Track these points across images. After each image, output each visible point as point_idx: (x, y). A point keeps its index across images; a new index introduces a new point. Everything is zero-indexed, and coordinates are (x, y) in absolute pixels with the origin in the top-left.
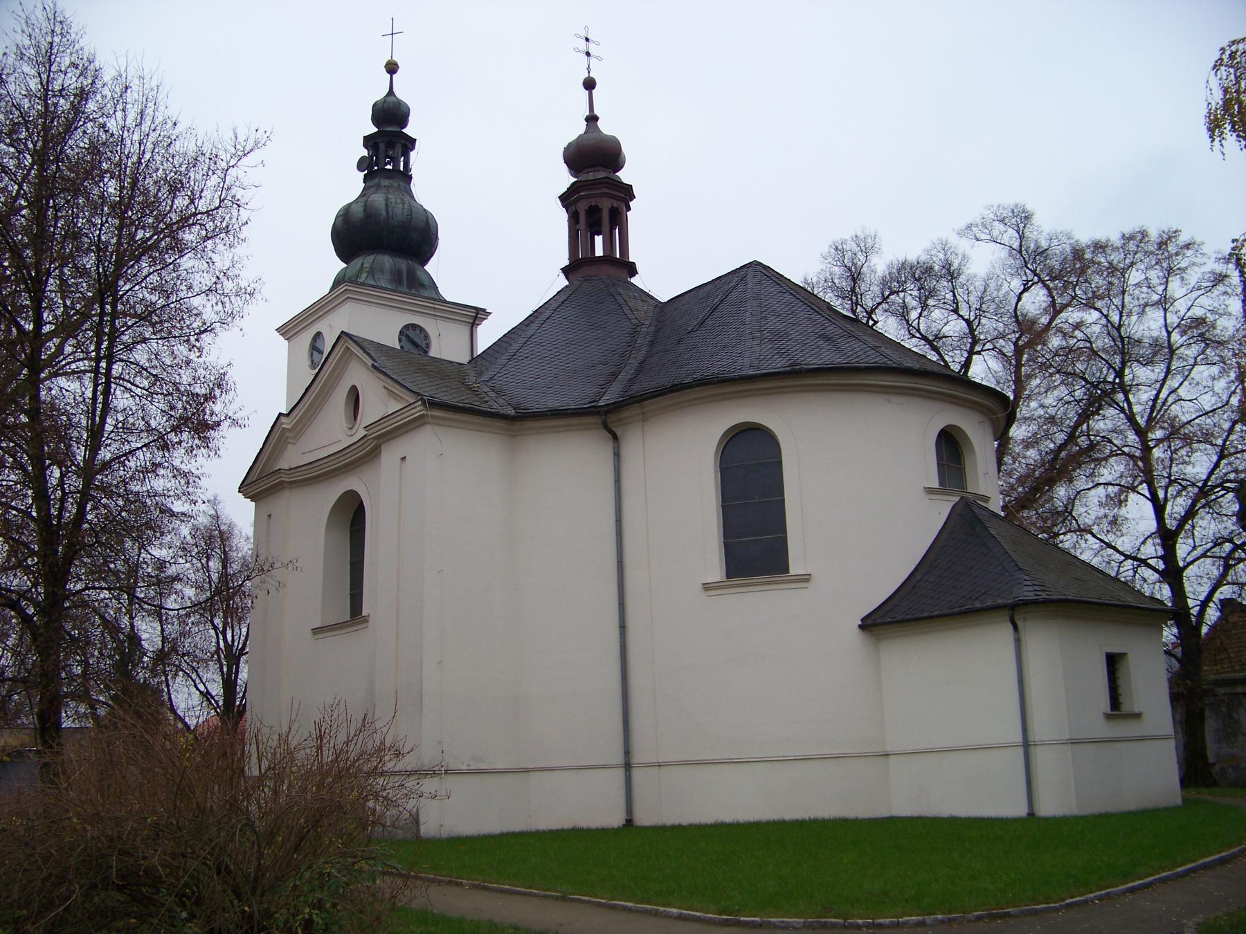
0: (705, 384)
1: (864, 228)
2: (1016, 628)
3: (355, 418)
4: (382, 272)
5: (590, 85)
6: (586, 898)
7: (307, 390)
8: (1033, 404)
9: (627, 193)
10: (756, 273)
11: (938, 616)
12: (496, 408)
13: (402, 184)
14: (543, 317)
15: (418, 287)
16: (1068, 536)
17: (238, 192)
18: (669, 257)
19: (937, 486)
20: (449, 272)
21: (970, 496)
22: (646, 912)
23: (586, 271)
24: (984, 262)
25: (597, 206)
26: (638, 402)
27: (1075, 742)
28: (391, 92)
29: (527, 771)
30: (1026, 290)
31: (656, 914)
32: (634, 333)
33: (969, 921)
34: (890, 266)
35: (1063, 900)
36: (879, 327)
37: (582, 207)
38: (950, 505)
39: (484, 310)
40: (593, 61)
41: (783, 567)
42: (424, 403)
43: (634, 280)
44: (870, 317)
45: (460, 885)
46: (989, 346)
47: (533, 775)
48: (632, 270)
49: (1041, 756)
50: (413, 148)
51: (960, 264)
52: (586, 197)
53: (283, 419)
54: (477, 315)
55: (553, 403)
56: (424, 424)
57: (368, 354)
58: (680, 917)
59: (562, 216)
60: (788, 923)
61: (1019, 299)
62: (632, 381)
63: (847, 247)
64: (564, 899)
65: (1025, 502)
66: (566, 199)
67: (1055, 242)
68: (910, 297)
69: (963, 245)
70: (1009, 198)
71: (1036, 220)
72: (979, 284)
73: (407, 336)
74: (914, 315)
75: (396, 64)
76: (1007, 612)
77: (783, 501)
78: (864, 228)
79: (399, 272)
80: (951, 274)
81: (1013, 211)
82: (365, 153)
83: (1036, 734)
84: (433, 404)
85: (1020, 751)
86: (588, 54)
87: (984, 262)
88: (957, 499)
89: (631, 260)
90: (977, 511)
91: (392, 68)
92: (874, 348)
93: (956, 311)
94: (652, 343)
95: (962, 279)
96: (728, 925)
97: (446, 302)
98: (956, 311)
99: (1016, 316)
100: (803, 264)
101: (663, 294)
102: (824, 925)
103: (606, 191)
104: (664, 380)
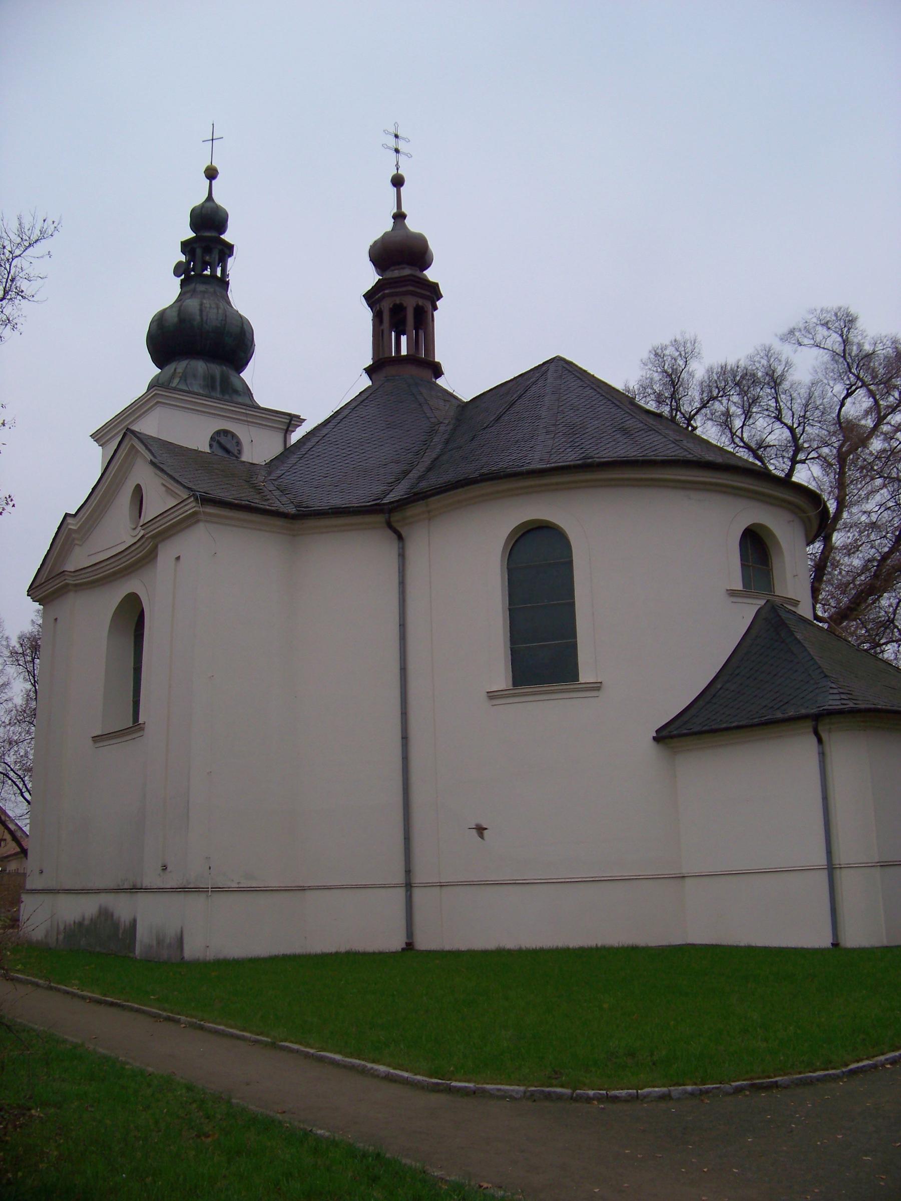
0: (500, 478)
1: (683, 333)
2: (820, 741)
3: (140, 517)
4: (195, 376)
5: (398, 182)
6: (295, 1046)
7: (94, 489)
8: (854, 510)
9: (433, 292)
10: (559, 370)
11: (738, 727)
12: (277, 505)
13: (218, 289)
14: (340, 417)
15: (236, 396)
16: (889, 646)
17: (23, 285)
18: (472, 357)
19: (740, 587)
20: (266, 379)
21: (776, 599)
22: (352, 1068)
23: (391, 370)
24: (806, 367)
26: (423, 499)
27: (884, 865)
28: (210, 198)
29: (303, 889)
30: (848, 395)
31: (364, 1072)
32: (432, 432)
33: (728, 1094)
34: (710, 370)
35: (847, 1065)
36: (698, 432)
37: (386, 305)
38: (755, 609)
39: (298, 417)
40: (402, 158)
41: (574, 677)
42: (196, 499)
43: (440, 382)
44: (689, 424)
45: (178, 1022)
46: (813, 455)
47: (308, 893)
48: (437, 371)
49: (847, 881)
50: (231, 254)
51: (783, 371)
53: (69, 520)
54: (292, 421)
55: (337, 501)
56: (198, 521)
57: (150, 451)
58: (388, 1078)
59: (366, 315)
60: (505, 1091)
61: (842, 404)
62: (421, 478)
63: (667, 352)
64: (273, 1045)
65: (843, 615)
66: (371, 297)
67: (880, 347)
68: (733, 403)
69: (786, 351)
70: (832, 300)
71: (860, 324)
72: (803, 391)
73: (219, 443)
74: (737, 423)
76: (810, 724)
77: (573, 604)
78: (683, 333)
79: (213, 378)
80: (774, 381)
81: (836, 315)
82: (183, 258)
83: (842, 856)
84: (206, 500)
85: (823, 876)
86: (397, 151)
87: (806, 367)
88: (762, 602)
89: (436, 360)
90: (784, 615)
91: (211, 174)
92: (675, 442)
93: (778, 418)
94: (447, 442)
95: (786, 385)
96: (439, 1091)
98: (778, 418)
99: (840, 423)
100: (622, 368)
101: (466, 394)
102: (548, 1096)
103: (411, 288)
104: (449, 475)
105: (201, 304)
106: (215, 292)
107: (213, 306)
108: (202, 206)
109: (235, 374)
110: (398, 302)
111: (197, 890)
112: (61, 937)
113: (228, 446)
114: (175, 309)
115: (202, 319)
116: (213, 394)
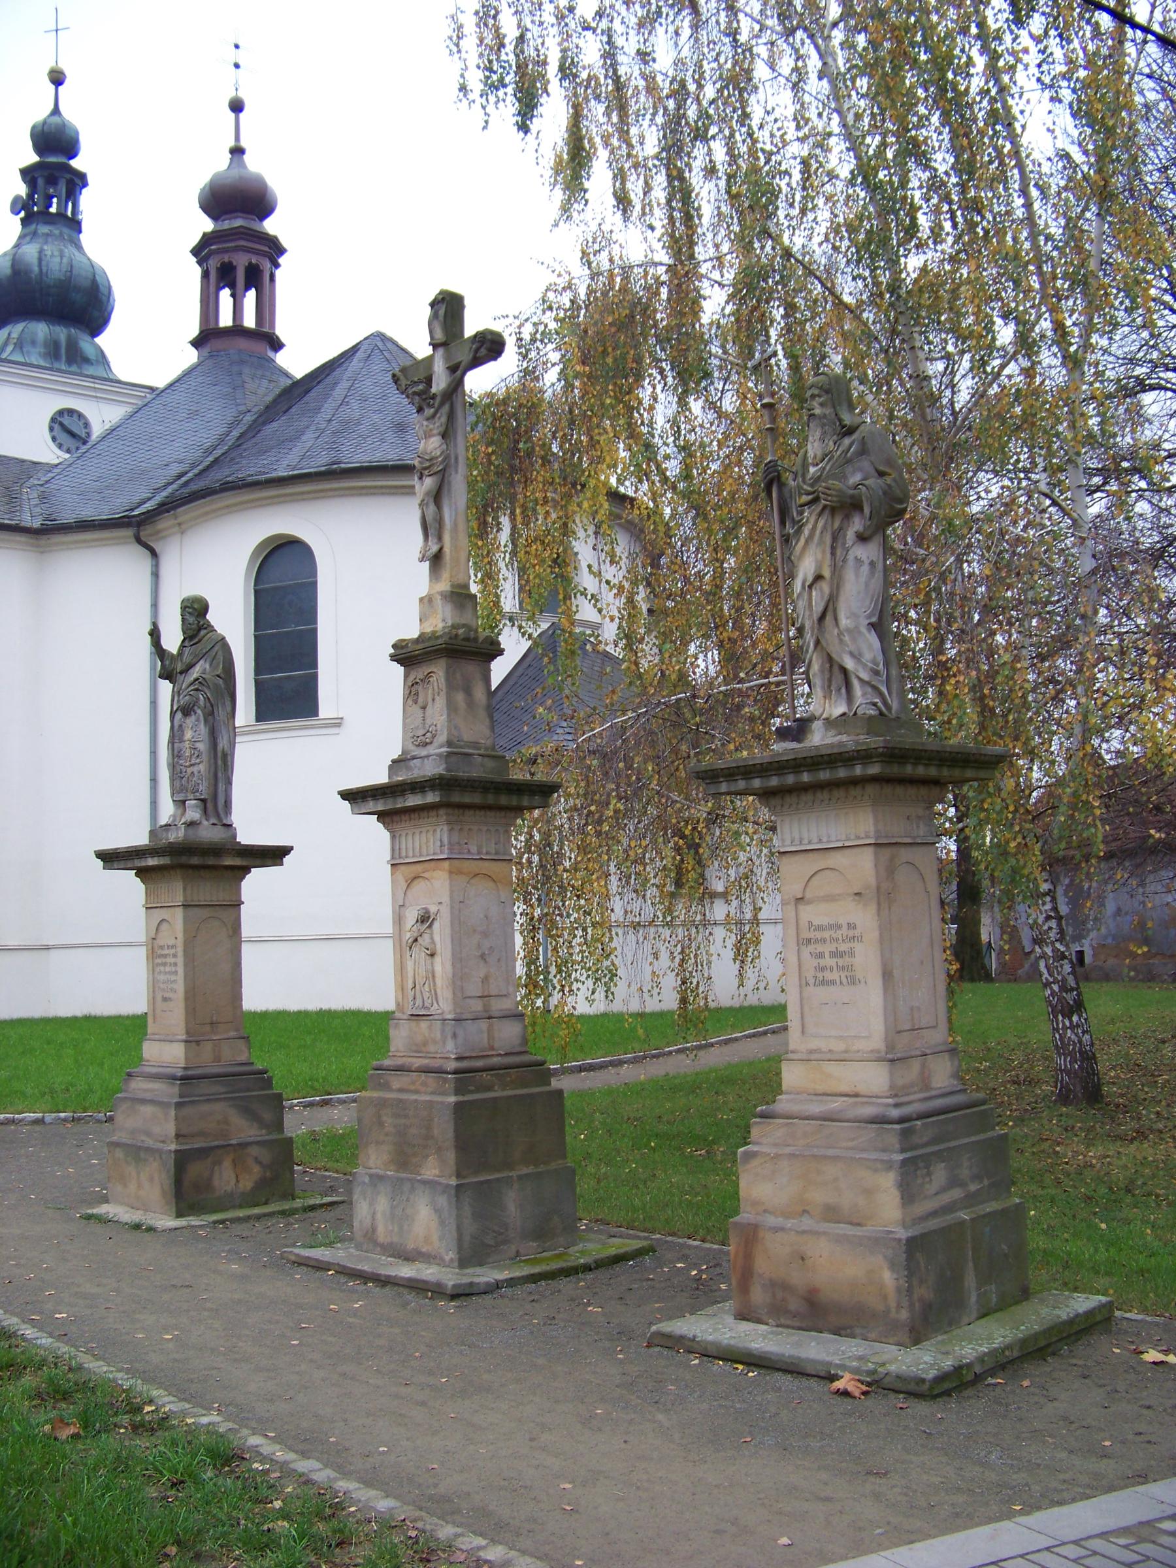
0: (239, 488)
4: (33, 343)
5: (237, 107)
13: (66, 231)
18: (311, 325)
25: (230, 263)
28: (56, 111)
29: (47, 948)
37: (214, 264)
52: (217, 252)
73: (61, 424)
75: (62, 73)
79: (56, 344)
91: (57, 79)
97: (120, 382)
103: (243, 243)
105: (41, 252)
106: (61, 234)
107: (56, 253)
108: (45, 122)
113: (75, 430)
114: (9, 258)
116: (56, 365)
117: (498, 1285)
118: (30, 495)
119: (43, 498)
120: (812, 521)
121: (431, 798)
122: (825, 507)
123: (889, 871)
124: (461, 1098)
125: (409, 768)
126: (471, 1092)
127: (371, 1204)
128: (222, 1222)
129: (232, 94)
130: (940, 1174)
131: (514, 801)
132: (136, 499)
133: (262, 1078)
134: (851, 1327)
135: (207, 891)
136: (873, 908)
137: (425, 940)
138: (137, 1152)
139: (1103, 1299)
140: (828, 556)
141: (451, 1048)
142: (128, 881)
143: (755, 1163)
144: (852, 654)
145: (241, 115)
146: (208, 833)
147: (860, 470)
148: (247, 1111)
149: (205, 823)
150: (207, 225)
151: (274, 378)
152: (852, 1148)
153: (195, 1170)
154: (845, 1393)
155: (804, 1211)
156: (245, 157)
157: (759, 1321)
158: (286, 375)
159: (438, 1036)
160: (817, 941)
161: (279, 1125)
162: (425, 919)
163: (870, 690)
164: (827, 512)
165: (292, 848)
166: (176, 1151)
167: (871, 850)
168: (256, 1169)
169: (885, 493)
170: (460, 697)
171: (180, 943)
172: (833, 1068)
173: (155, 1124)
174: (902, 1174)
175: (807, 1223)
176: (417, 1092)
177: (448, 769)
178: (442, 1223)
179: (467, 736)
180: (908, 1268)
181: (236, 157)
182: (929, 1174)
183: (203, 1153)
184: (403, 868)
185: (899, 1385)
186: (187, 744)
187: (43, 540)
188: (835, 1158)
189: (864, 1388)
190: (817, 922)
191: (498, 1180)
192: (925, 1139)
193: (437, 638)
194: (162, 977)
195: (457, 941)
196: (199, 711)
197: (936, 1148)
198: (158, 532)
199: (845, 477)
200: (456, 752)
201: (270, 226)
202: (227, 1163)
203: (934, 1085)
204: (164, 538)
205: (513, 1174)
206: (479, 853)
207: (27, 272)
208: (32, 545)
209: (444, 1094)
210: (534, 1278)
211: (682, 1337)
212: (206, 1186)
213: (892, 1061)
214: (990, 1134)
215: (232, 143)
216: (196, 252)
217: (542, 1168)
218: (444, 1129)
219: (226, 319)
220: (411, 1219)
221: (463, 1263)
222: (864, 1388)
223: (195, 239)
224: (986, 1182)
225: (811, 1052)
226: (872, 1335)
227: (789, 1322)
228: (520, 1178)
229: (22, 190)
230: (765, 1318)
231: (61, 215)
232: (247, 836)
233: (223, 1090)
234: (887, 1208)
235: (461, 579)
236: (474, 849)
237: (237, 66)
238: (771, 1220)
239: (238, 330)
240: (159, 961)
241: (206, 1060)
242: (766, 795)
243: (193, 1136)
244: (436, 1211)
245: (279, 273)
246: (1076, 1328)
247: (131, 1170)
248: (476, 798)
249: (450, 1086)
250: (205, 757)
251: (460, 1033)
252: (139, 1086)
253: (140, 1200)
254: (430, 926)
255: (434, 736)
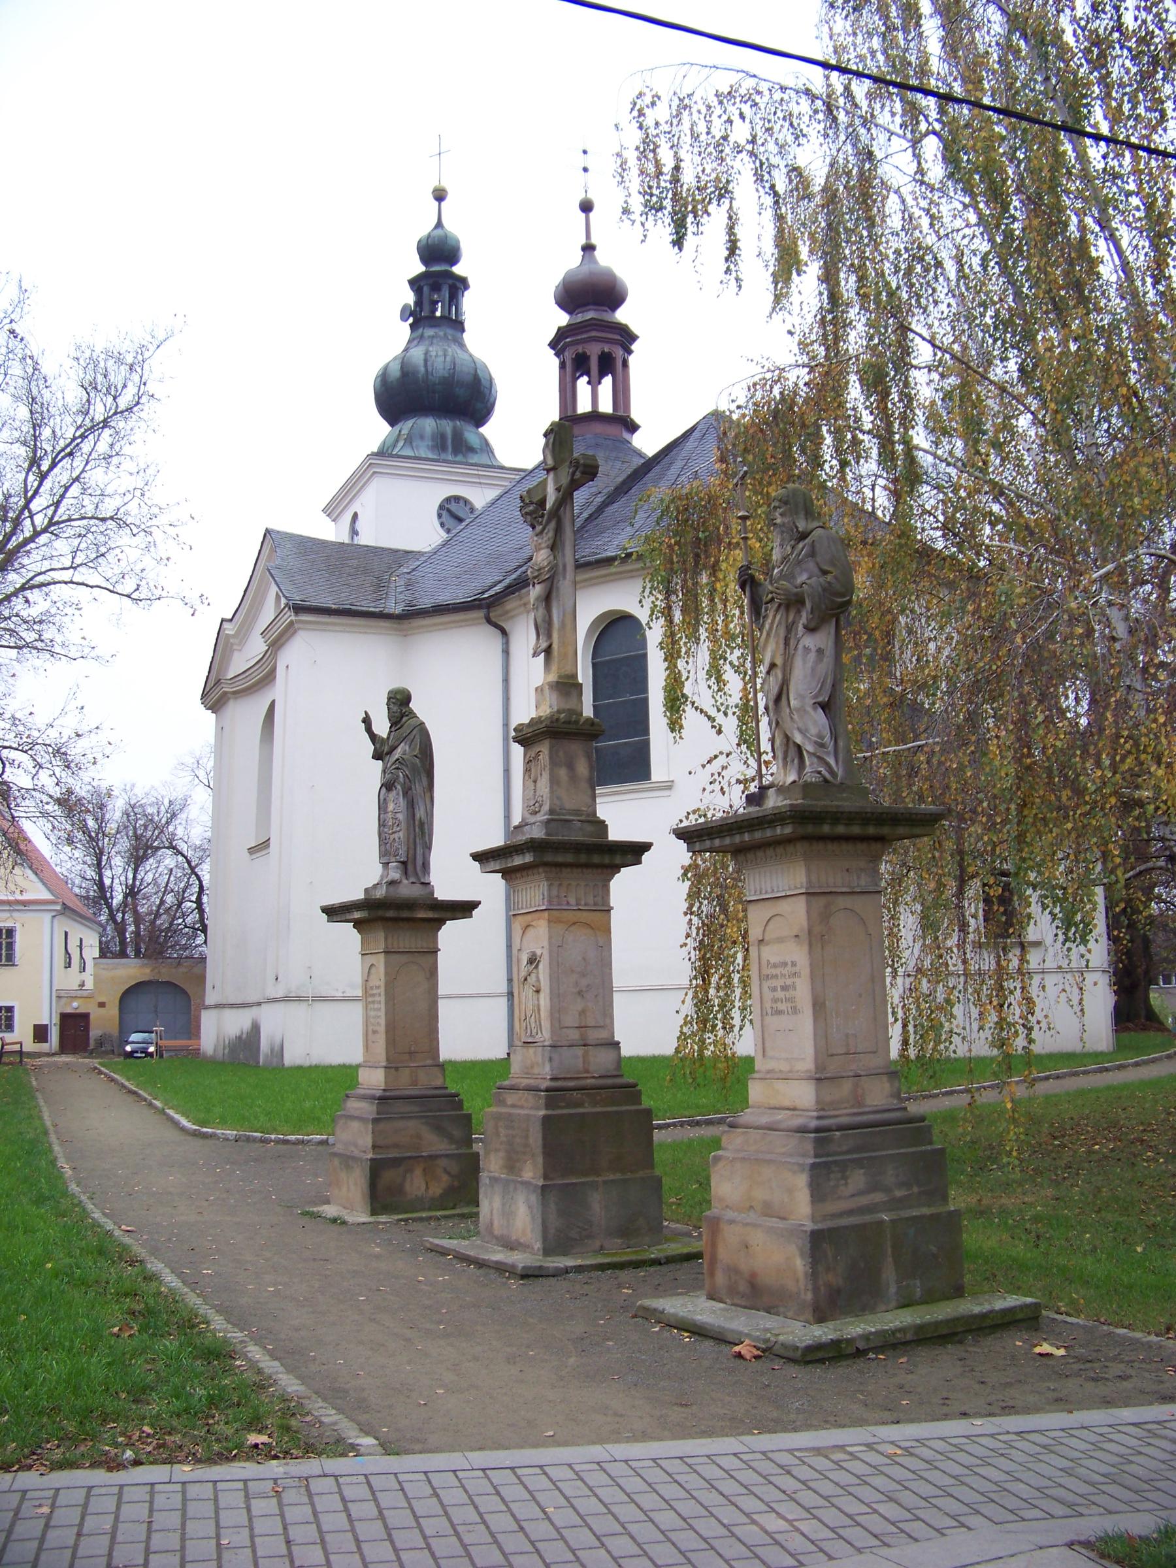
13: (450, 332)
28: (439, 225)
37: (569, 355)
53: (226, 625)
56: (295, 632)
73: (449, 511)
79: (443, 437)
84: (298, 609)
91: (440, 196)
97: (503, 468)
103: (594, 334)
105: (426, 354)
107: (440, 353)
108: (429, 236)
109: (473, 429)
110: (580, 351)
111: (299, 999)
112: (226, 1051)
114: (398, 362)
115: (427, 370)
116: (443, 456)
117: (567, 1271)
118: (398, 583)
119: (408, 586)
120: (771, 617)
121: (528, 858)
122: (780, 605)
123: (825, 916)
124: (549, 1112)
125: (523, 834)
126: (563, 1108)
127: (490, 1203)
128: (406, 1220)
129: (582, 196)
130: (858, 1179)
131: (607, 860)
132: (489, 582)
133: (454, 1101)
134: (777, 1306)
135: (408, 940)
136: (806, 948)
137: (532, 979)
138: (347, 1160)
139: (1029, 1300)
140: (782, 646)
141: (546, 1070)
142: (347, 934)
143: (721, 1164)
144: (799, 729)
145: (591, 215)
146: (407, 890)
147: (806, 570)
148: (439, 1129)
149: (405, 882)
150: (563, 319)
151: (628, 459)
152: (784, 1154)
153: (389, 1176)
154: (739, 1355)
155: (751, 1207)
156: (596, 253)
157: (721, 1301)
158: (640, 454)
159: (540, 1060)
160: (773, 977)
161: (469, 1142)
162: (533, 960)
163: (815, 760)
164: (782, 608)
165: (479, 903)
166: (371, 1160)
167: (803, 898)
168: (445, 1178)
169: (824, 590)
170: (563, 773)
171: (382, 984)
172: (780, 1085)
173: (357, 1137)
174: (811, 1176)
175: (752, 1217)
176: (522, 1107)
177: (547, 834)
178: (533, 1218)
179: (569, 804)
180: (813, 1256)
181: (587, 253)
182: (845, 1178)
183: (396, 1162)
184: (519, 918)
185: (782, 1352)
186: (390, 815)
187: (406, 624)
188: (770, 1162)
189: (759, 1353)
190: (774, 960)
191: (583, 1184)
192: (845, 1148)
193: (542, 722)
194: (372, 1013)
195: (555, 979)
196: (399, 787)
197: (855, 1156)
198: (507, 612)
199: (794, 577)
200: (556, 820)
201: (622, 315)
202: (418, 1172)
203: (869, 1102)
204: (512, 617)
205: (600, 1179)
206: (577, 904)
207: (415, 373)
208: (396, 630)
209: (538, 1108)
210: (602, 1267)
211: (655, 1310)
212: (399, 1190)
213: (817, 1079)
214: (919, 1149)
215: (583, 241)
216: (553, 345)
217: (628, 1176)
218: (536, 1138)
219: (584, 405)
220: (512, 1213)
221: (547, 1252)
222: (759, 1353)
223: (551, 334)
224: (915, 1189)
225: (769, 1072)
226: (790, 1314)
227: (739, 1302)
228: (605, 1182)
229: (409, 298)
230: (724, 1298)
231: (445, 318)
232: (442, 893)
233: (417, 1109)
234: (801, 1207)
235: (568, 670)
236: (572, 901)
237: (585, 170)
238: (730, 1214)
239: (594, 416)
240: (370, 999)
241: (403, 1083)
242: (738, 852)
243: (387, 1147)
244: (529, 1207)
245: (632, 359)
246: (989, 1322)
247: (343, 1175)
248: (569, 858)
249: (542, 1102)
250: (403, 825)
251: (555, 1056)
252: (354, 1105)
253: (348, 1200)
254: (536, 967)
255: (541, 806)
